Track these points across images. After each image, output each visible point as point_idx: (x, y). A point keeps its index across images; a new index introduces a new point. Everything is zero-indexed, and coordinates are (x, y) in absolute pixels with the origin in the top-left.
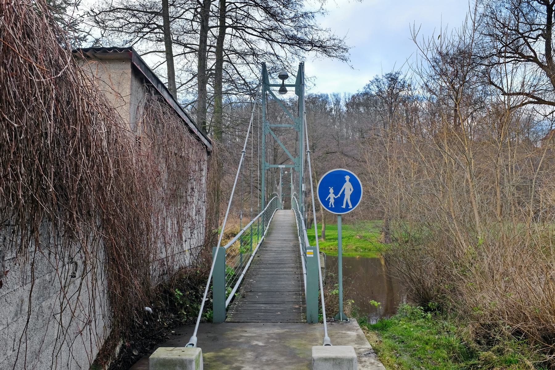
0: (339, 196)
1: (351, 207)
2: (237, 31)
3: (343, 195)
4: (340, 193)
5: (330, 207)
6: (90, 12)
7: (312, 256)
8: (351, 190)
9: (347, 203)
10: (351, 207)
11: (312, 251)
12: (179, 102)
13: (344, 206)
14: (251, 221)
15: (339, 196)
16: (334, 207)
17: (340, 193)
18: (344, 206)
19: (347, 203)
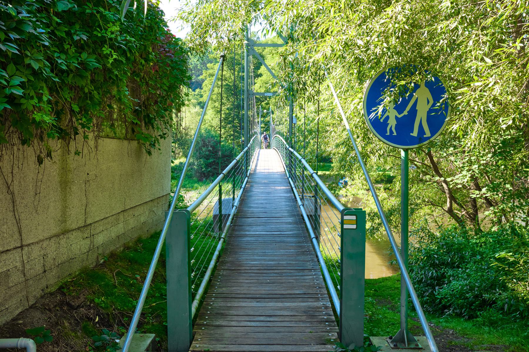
0: (405, 113)
1: (428, 134)
2: (17, 69)
3: (413, 112)
4: (408, 108)
5: (388, 134)
6: (409, 265)
7: (354, 227)
8: (428, 102)
9: (421, 126)
10: (428, 134)
11: (354, 218)
12: (205, 117)
13: (415, 134)
14: (241, 151)
15: (405, 113)
16: (395, 134)
17: (408, 108)
18: (415, 134)
19: (421, 126)
